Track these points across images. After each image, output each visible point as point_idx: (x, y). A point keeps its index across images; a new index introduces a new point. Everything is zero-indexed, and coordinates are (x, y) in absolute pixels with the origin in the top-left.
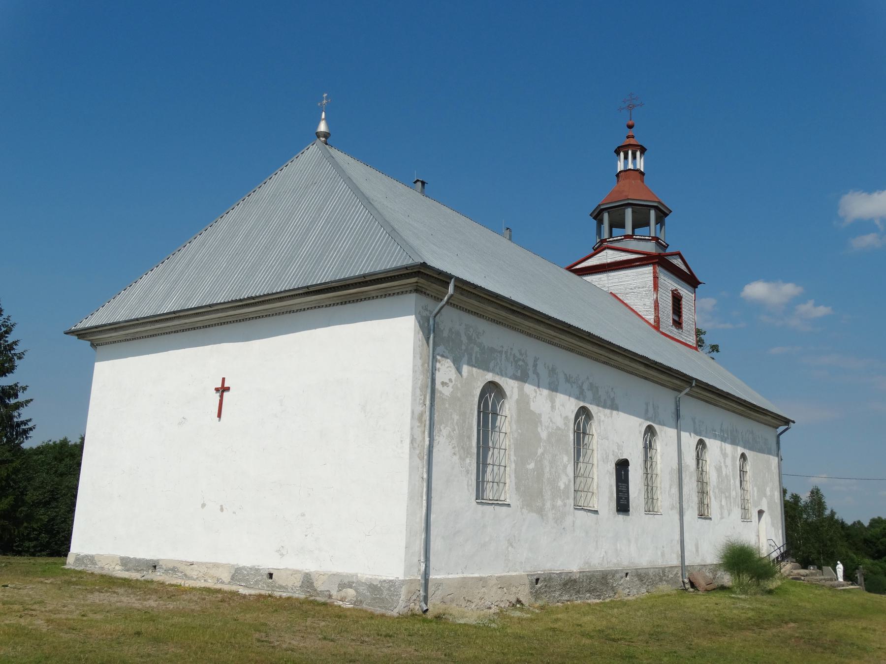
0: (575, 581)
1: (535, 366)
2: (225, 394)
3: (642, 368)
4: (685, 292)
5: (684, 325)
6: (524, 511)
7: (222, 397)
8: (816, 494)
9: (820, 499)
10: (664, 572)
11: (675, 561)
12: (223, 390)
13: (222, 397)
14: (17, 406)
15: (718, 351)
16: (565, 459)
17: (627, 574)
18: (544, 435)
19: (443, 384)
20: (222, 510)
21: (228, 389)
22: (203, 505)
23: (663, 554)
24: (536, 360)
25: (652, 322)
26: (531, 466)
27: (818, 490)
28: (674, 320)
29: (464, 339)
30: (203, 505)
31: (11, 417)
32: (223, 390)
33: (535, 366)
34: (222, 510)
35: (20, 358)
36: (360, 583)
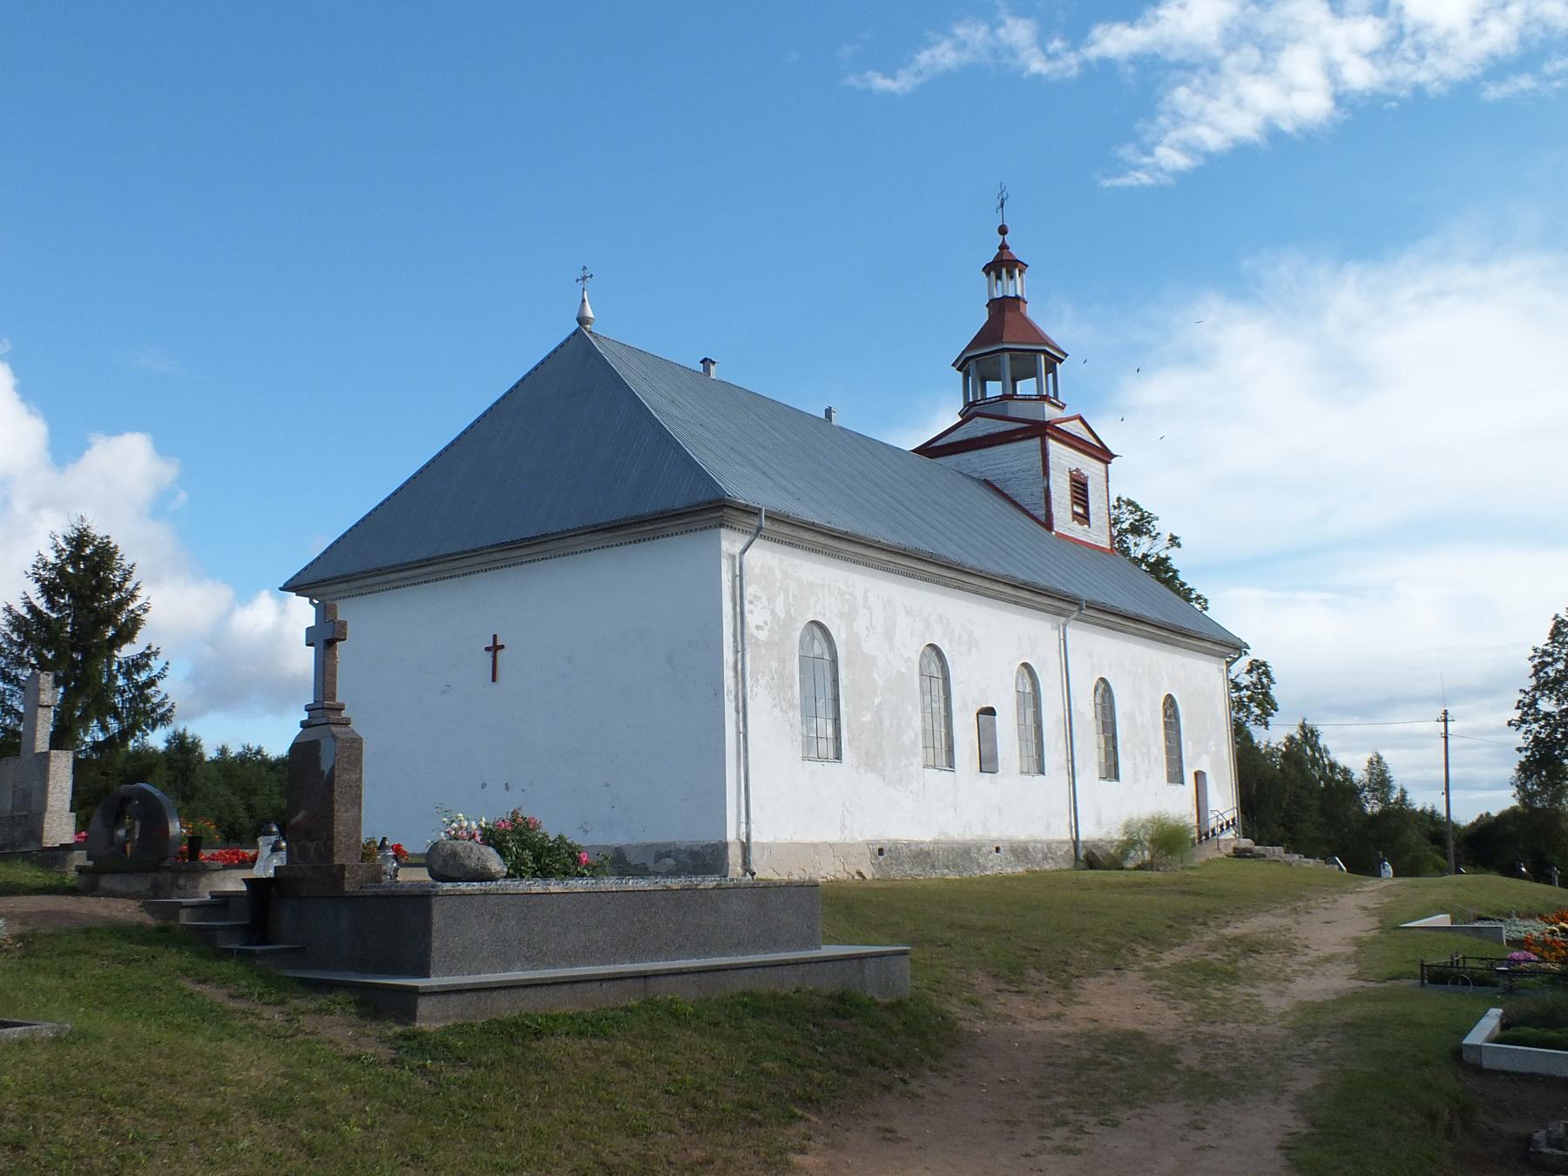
0: (928, 853)
1: (866, 598)
2: (500, 652)
3: (1009, 590)
4: (1091, 468)
5: (1092, 519)
6: (861, 770)
7: (495, 657)
8: (1377, 768)
9: (1383, 772)
10: (1049, 849)
11: (1065, 834)
12: (495, 648)
13: (495, 657)
14: (151, 682)
15: (1179, 545)
16: (910, 708)
17: (998, 850)
18: (880, 683)
19: (758, 627)
20: (507, 788)
21: (502, 647)
22: (484, 786)
23: (1048, 827)
24: (866, 591)
25: (1043, 519)
26: (867, 718)
27: (1379, 758)
28: (1075, 513)
29: (779, 575)
30: (484, 786)
31: (147, 699)
32: (495, 648)
33: (866, 598)
34: (507, 788)
35: (146, 610)
36: (679, 851)
